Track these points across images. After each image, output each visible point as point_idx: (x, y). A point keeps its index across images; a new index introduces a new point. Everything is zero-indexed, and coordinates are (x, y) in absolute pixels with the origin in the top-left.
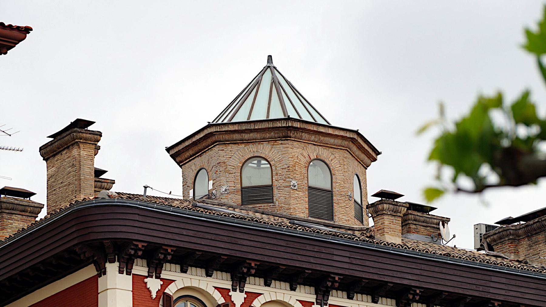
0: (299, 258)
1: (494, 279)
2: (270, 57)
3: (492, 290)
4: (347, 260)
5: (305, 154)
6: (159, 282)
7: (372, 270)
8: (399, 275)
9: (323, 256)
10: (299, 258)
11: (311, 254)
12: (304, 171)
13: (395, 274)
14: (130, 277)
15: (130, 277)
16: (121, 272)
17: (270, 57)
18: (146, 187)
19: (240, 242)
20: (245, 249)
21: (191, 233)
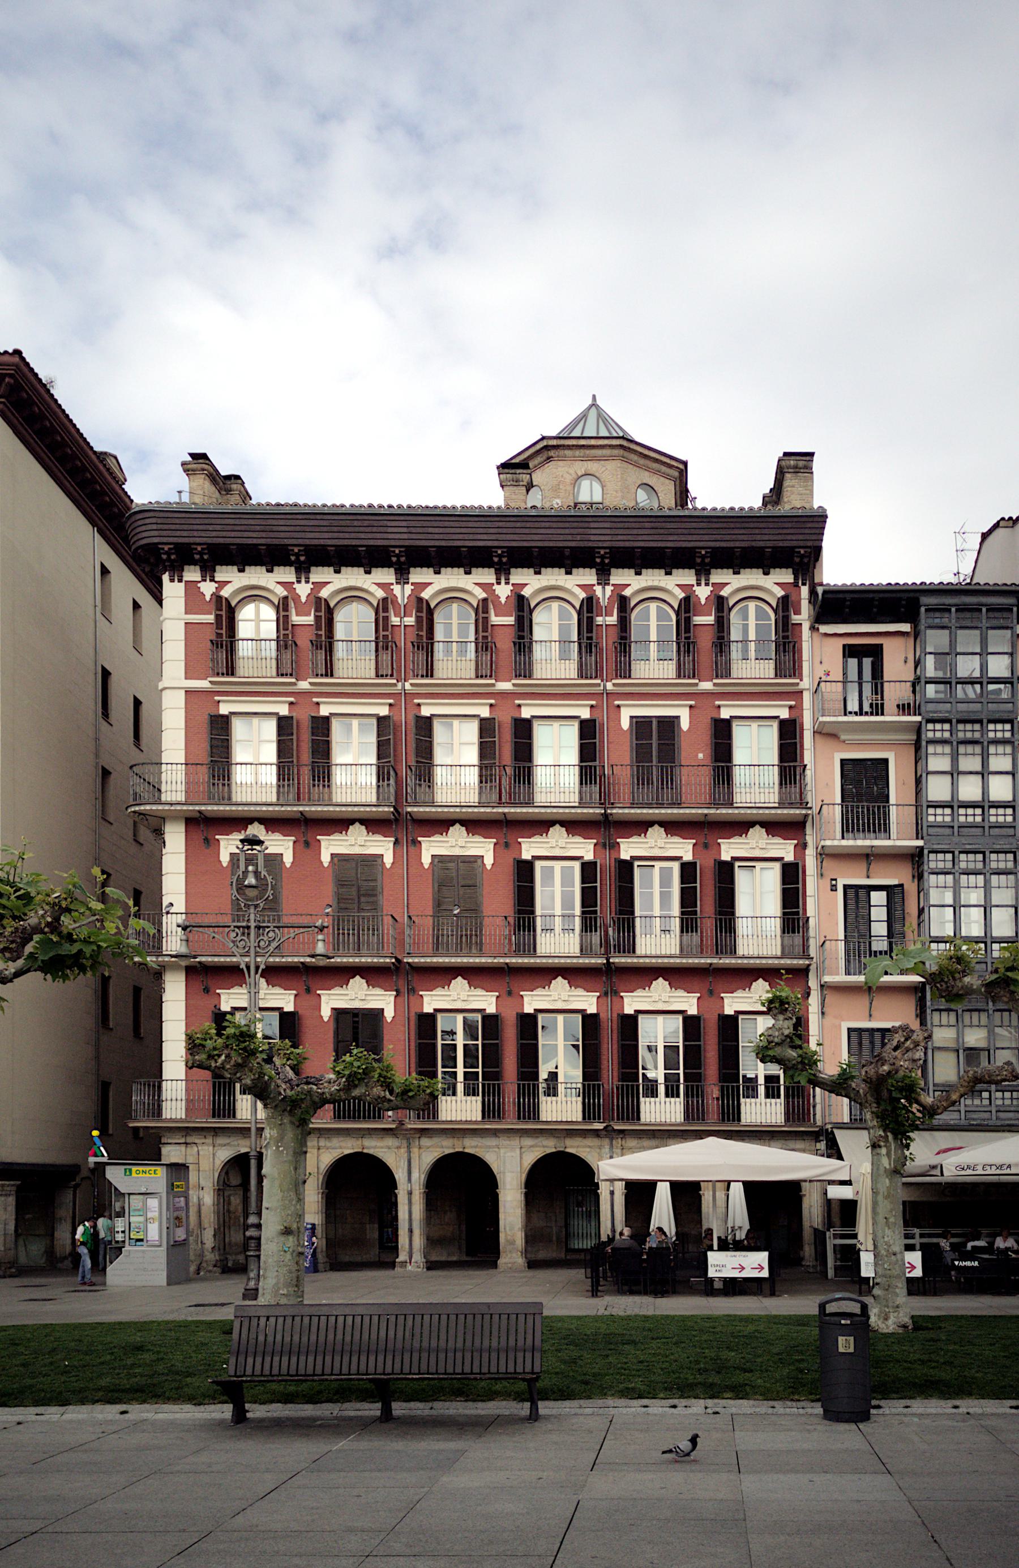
0: (347, 535)
1: (592, 525)
2: (594, 397)
3: (592, 538)
4: (405, 530)
5: (572, 472)
6: (214, 585)
7: (436, 537)
8: (471, 537)
9: (375, 529)
10: (347, 535)
11: (362, 529)
12: (569, 488)
13: (466, 537)
14: (183, 584)
15: (183, 584)
16: (172, 581)
17: (594, 397)
18: (180, 492)
19: (275, 528)
20: (282, 535)
21: (218, 527)
